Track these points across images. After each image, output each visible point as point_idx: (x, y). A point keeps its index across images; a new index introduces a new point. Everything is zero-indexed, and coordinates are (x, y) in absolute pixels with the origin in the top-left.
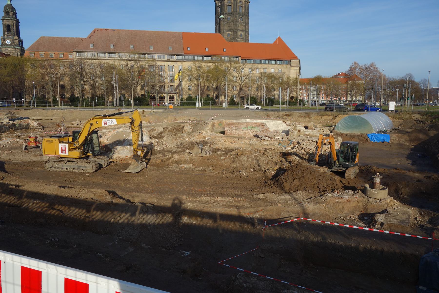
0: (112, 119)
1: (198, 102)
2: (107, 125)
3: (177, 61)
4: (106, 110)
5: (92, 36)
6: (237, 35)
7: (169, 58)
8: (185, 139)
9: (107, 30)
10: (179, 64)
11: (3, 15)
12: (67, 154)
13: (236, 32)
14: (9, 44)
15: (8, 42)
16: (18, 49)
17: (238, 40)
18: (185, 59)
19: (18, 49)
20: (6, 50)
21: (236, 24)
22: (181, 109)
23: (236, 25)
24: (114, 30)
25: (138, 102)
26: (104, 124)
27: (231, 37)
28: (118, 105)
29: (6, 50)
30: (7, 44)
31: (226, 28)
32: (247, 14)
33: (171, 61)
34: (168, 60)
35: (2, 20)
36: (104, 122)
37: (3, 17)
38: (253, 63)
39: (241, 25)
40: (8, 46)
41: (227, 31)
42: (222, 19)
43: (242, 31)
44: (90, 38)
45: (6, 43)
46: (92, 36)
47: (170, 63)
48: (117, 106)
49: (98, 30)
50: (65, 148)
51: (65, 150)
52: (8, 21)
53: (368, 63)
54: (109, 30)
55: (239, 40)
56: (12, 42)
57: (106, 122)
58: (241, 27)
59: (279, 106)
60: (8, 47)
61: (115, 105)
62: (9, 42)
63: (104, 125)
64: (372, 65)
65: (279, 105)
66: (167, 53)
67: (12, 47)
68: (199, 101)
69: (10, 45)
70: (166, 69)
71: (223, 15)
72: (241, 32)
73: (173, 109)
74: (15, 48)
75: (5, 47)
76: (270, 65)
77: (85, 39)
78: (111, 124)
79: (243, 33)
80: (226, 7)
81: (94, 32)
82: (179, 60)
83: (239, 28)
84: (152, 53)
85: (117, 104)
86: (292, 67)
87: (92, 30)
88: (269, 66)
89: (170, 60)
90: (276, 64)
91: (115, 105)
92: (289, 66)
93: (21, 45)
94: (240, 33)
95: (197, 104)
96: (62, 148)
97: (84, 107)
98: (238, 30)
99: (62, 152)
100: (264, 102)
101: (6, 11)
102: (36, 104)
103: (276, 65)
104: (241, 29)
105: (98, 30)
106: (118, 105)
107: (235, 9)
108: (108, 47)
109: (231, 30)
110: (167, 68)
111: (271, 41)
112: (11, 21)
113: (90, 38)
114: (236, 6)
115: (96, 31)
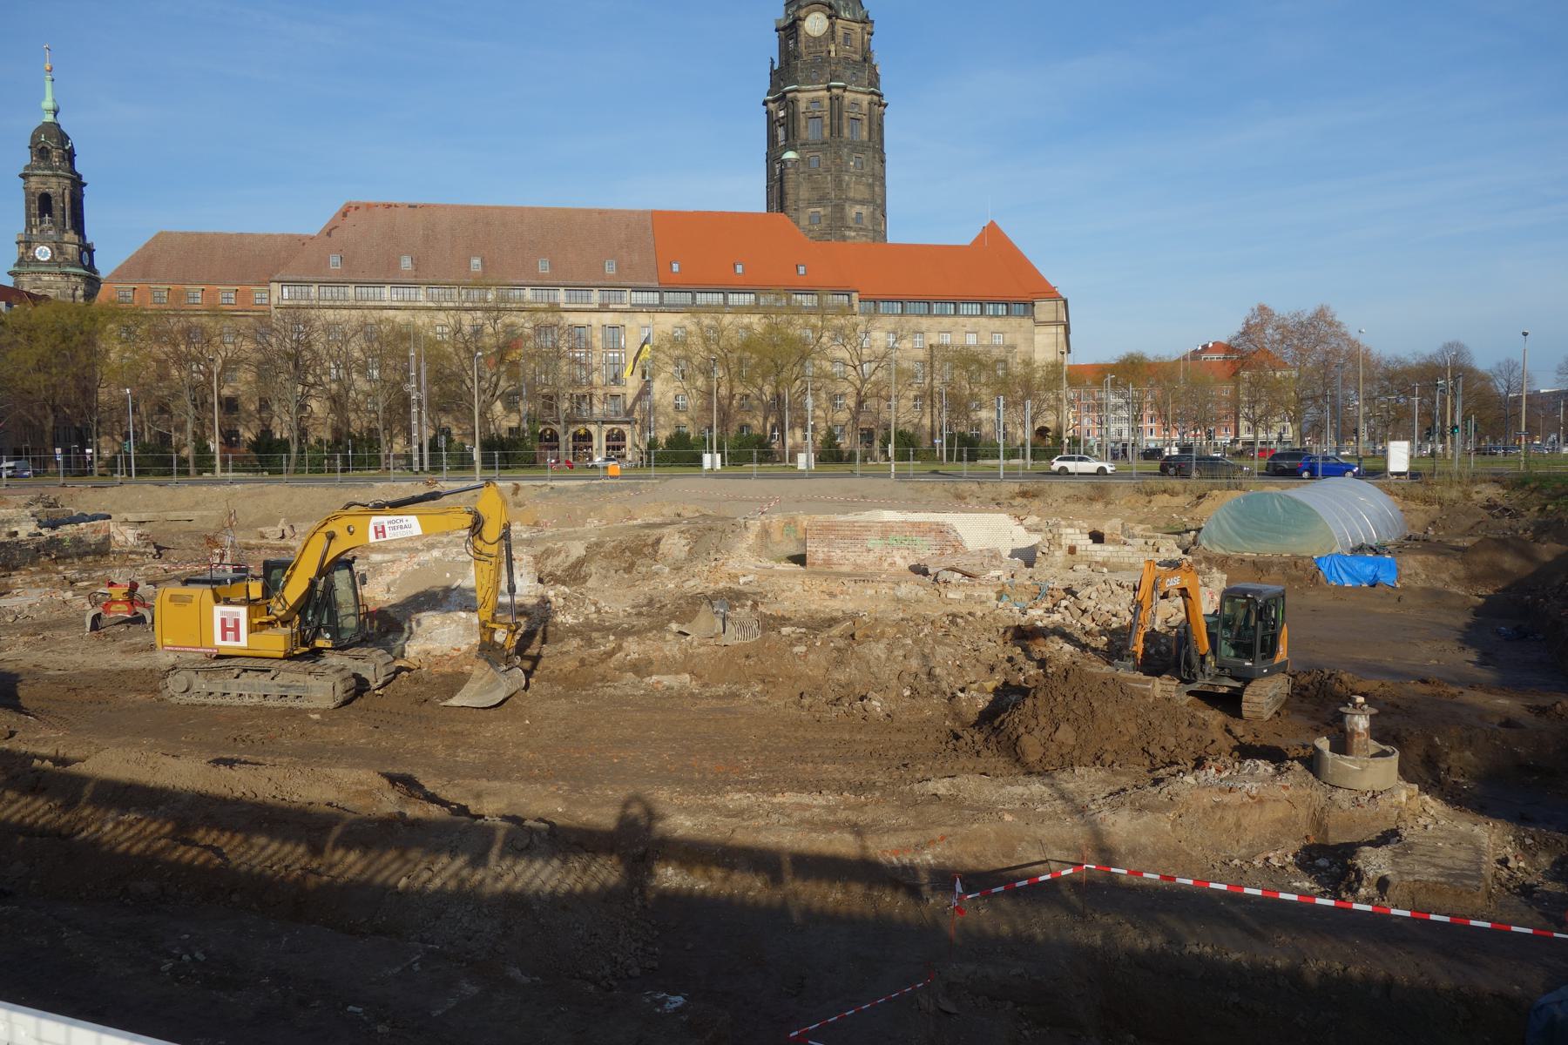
0: (404, 518)
1: (711, 452)
2: (388, 538)
3: (636, 309)
4: (384, 484)
5: (336, 227)
6: (842, 218)
7: (606, 301)
8: (663, 583)
9: (390, 206)
10: (643, 318)
11: (29, 162)
12: (243, 642)
13: (839, 208)
14: (45, 259)
15: (41, 251)
16: (75, 275)
17: (847, 233)
18: (661, 304)
19: (75, 275)
20: (35, 280)
21: (841, 181)
22: (648, 477)
23: (838, 182)
24: (415, 207)
25: (497, 456)
26: (377, 533)
27: (824, 223)
28: (426, 466)
29: (35, 280)
30: (38, 261)
31: (804, 193)
32: (875, 147)
33: (615, 311)
34: (603, 308)
35: (24, 176)
36: (376, 528)
37: (27, 167)
38: (902, 314)
39: (856, 183)
40: (42, 265)
41: (810, 204)
42: (789, 164)
43: (862, 202)
44: (329, 234)
45: (34, 257)
46: (336, 227)
47: (608, 318)
48: (422, 469)
49: (357, 208)
50: (237, 622)
51: (236, 629)
52: (44, 179)
53: (1308, 308)
54: (396, 206)
55: (853, 234)
56: (56, 252)
57: (383, 527)
58: (857, 190)
59: (995, 462)
60: (43, 269)
61: (416, 468)
62: (46, 252)
63: (377, 537)
64: (1321, 314)
65: (998, 457)
66: (600, 283)
67: (57, 269)
68: (712, 448)
69: (48, 261)
70: (596, 336)
71: (795, 150)
72: (858, 208)
73: (622, 477)
74: (67, 275)
75: (32, 269)
76: (960, 320)
77: (312, 238)
78: (400, 534)
79: (865, 210)
80: (803, 123)
81: (345, 215)
82: (642, 305)
83: (851, 195)
84: (548, 282)
85: (421, 463)
86: (1038, 324)
87: (337, 207)
88: (957, 323)
89: (611, 306)
90: (982, 314)
91: (416, 468)
92: (1028, 322)
93: (87, 264)
94: (852, 211)
95: (707, 458)
96: (223, 621)
97: (307, 475)
98: (847, 199)
99: (224, 638)
100: (945, 448)
101: (40, 146)
102: (136, 466)
103: (983, 320)
104: (859, 197)
105: (357, 208)
106: (426, 466)
107: (836, 130)
108: (394, 265)
109: (821, 200)
110: (600, 336)
111: (964, 236)
112: (54, 180)
113: (329, 234)
114: (840, 118)
115: (352, 210)
